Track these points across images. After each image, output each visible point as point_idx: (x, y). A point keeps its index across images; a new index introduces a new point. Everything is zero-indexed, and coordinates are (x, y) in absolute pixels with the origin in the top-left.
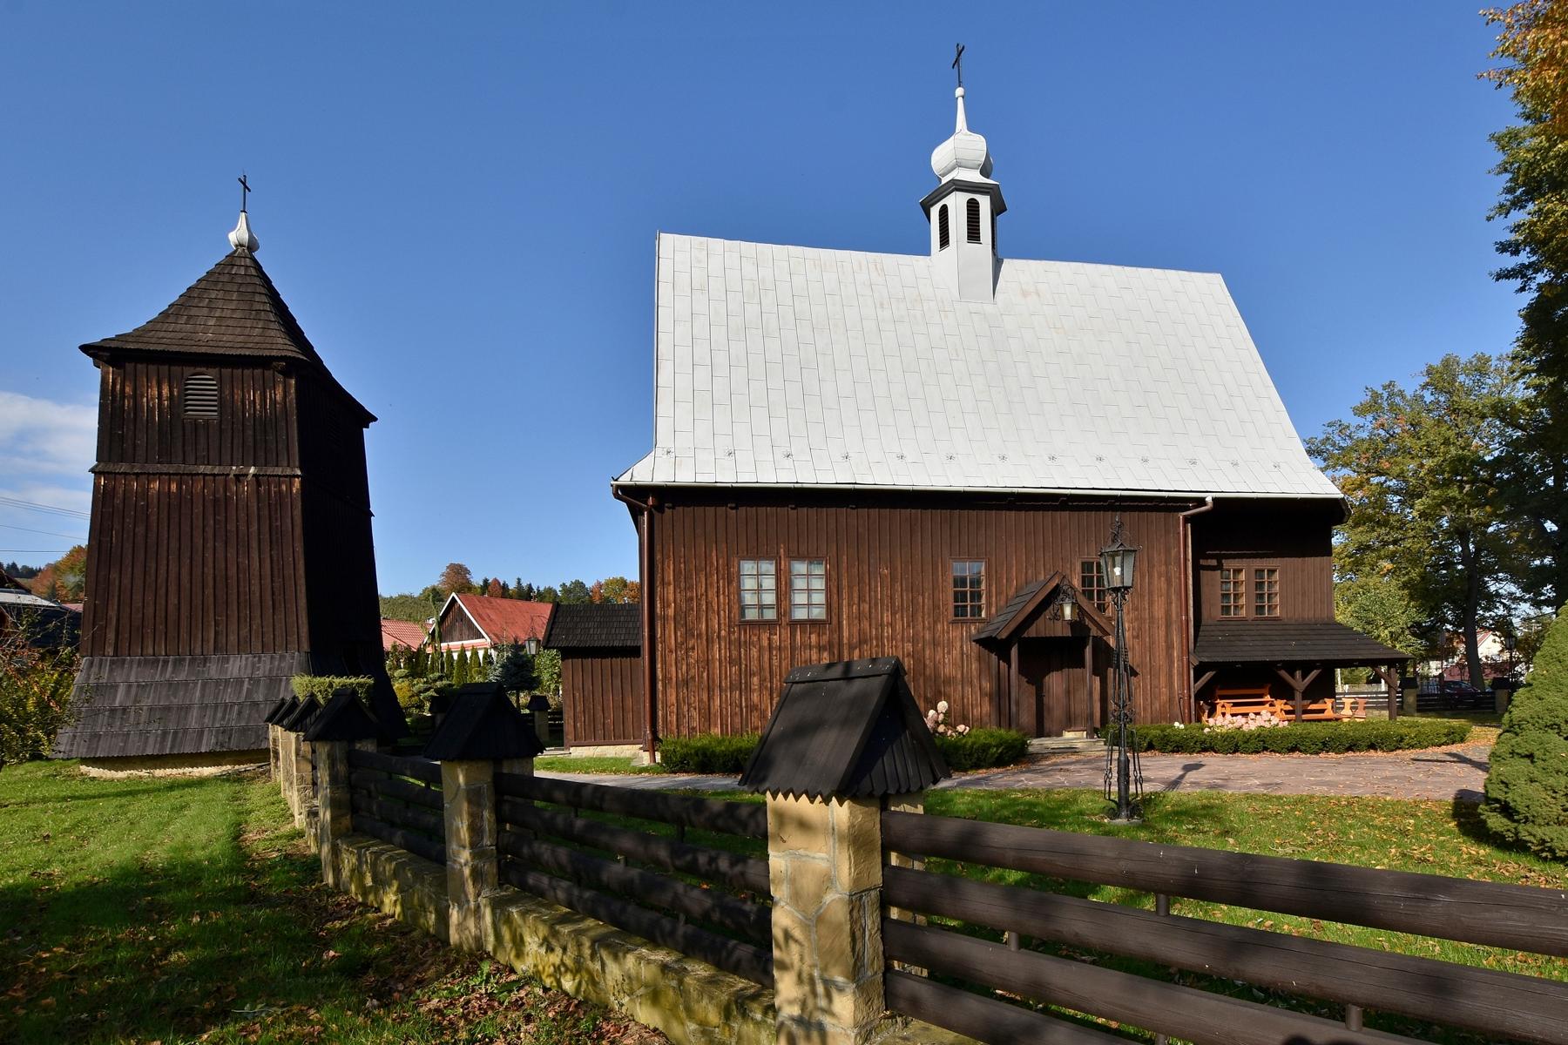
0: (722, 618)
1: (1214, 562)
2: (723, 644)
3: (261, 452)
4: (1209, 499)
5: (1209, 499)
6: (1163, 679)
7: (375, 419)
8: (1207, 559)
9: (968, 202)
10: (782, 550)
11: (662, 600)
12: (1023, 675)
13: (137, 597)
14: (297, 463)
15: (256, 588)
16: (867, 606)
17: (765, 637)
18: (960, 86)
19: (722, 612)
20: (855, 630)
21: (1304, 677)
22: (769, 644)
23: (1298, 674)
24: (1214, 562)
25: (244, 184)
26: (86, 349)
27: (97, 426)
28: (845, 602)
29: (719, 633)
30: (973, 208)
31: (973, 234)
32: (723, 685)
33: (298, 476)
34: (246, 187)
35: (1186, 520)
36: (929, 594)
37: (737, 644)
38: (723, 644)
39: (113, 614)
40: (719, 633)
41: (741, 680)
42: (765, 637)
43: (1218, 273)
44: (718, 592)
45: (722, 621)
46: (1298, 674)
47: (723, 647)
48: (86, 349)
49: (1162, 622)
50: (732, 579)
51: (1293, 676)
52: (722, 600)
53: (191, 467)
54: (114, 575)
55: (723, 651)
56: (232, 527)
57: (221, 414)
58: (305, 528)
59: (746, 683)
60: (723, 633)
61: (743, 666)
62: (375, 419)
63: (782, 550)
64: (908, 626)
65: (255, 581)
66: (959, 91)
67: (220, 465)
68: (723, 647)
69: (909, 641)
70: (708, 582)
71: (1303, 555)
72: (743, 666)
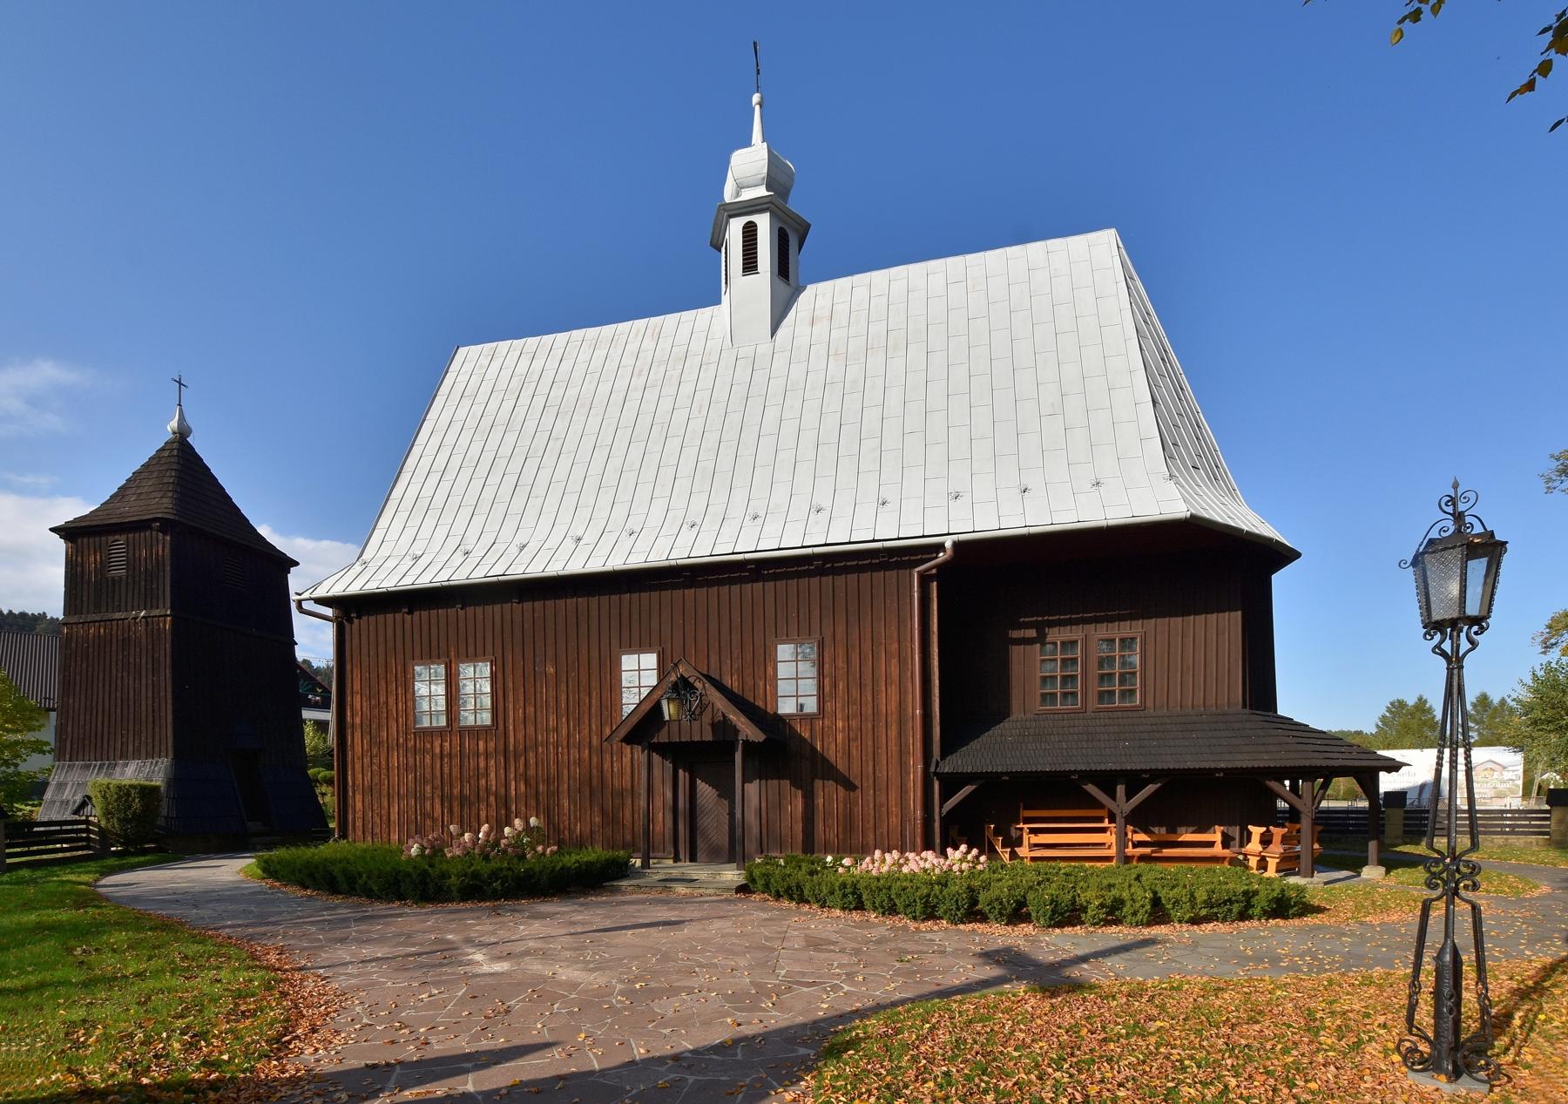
0: (400, 726)
1: (1032, 633)
2: (401, 752)
3: (149, 600)
4: (948, 545)
5: (948, 545)
6: (894, 796)
7: (296, 564)
8: (1020, 629)
9: (744, 228)
10: (452, 653)
11: (352, 709)
12: (797, 788)
13: (82, 717)
14: (169, 605)
15: (144, 707)
16: (532, 709)
17: (437, 744)
18: (758, 92)
19: (400, 720)
20: (520, 736)
21: (1129, 796)
22: (441, 751)
23: (1120, 790)
24: (1032, 633)
25: (180, 384)
26: (52, 530)
27: (64, 589)
28: (511, 706)
29: (398, 740)
30: (750, 232)
31: (750, 265)
32: (402, 792)
33: (168, 616)
34: (180, 384)
35: (925, 580)
36: (597, 694)
37: (413, 752)
38: (401, 752)
39: (69, 729)
40: (398, 740)
41: (416, 788)
42: (437, 744)
43: (1109, 227)
44: (396, 699)
45: (401, 729)
46: (1120, 790)
47: (401, 754)
48: (52, 530)
49: (893, 718)
50: (407, 684)
51: (1113, 796)
52: (400, 708)
53: (111, 615)
54: (71, 701)
55: (401, 759)
56: (131, 660)
57: (127, 572)
58: (173, 659)
59: (420, 791)
60: (401, 740)
61: (418, 774)
62: (296, 564)
63: (452, 653)
64: (574, 730)
65: (143, 703)
66: (756, 98)
67: (126, 611)
68: (401, 754)
69: (575, 747)
70: (389, 689)
71: (1185, 612)
72: (418, 774)
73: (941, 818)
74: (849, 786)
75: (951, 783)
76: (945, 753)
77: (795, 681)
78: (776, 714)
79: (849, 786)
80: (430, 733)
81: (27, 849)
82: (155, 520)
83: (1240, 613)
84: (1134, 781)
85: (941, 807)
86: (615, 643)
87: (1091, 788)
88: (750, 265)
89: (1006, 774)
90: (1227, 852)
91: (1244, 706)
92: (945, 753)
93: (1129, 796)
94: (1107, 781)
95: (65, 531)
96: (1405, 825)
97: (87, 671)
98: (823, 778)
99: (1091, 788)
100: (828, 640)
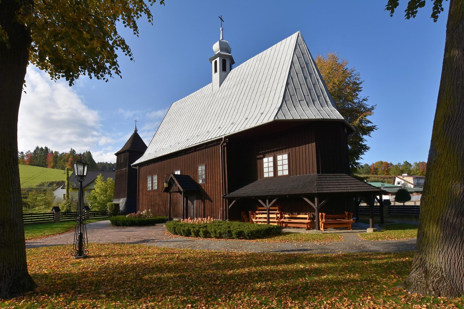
31: (216, 71)
73: (228, 210)
74: (211, 201)
75: (230, 200)
76: (229, 193)
77: (269, 166)
78: (198, 184)
79: (211, 201)
80: (149, 191)
81: (402, 204)
82: (126, 150)
83: (314, 144)
84: (271, 198)
85: (228, 207)
86: (174, 169)
87: (260, 201)
88: (216, 71)
89: (287, 195)
90: (277, 221)
91: (318, 172)
92: (229, 193)
93: (269, 203)
94: (264, 198)
95: (116, 154)
96: (419, 211)
97: (452, 123)
98: (207, 199)
99: (260, 201)
100: (207, 164)
